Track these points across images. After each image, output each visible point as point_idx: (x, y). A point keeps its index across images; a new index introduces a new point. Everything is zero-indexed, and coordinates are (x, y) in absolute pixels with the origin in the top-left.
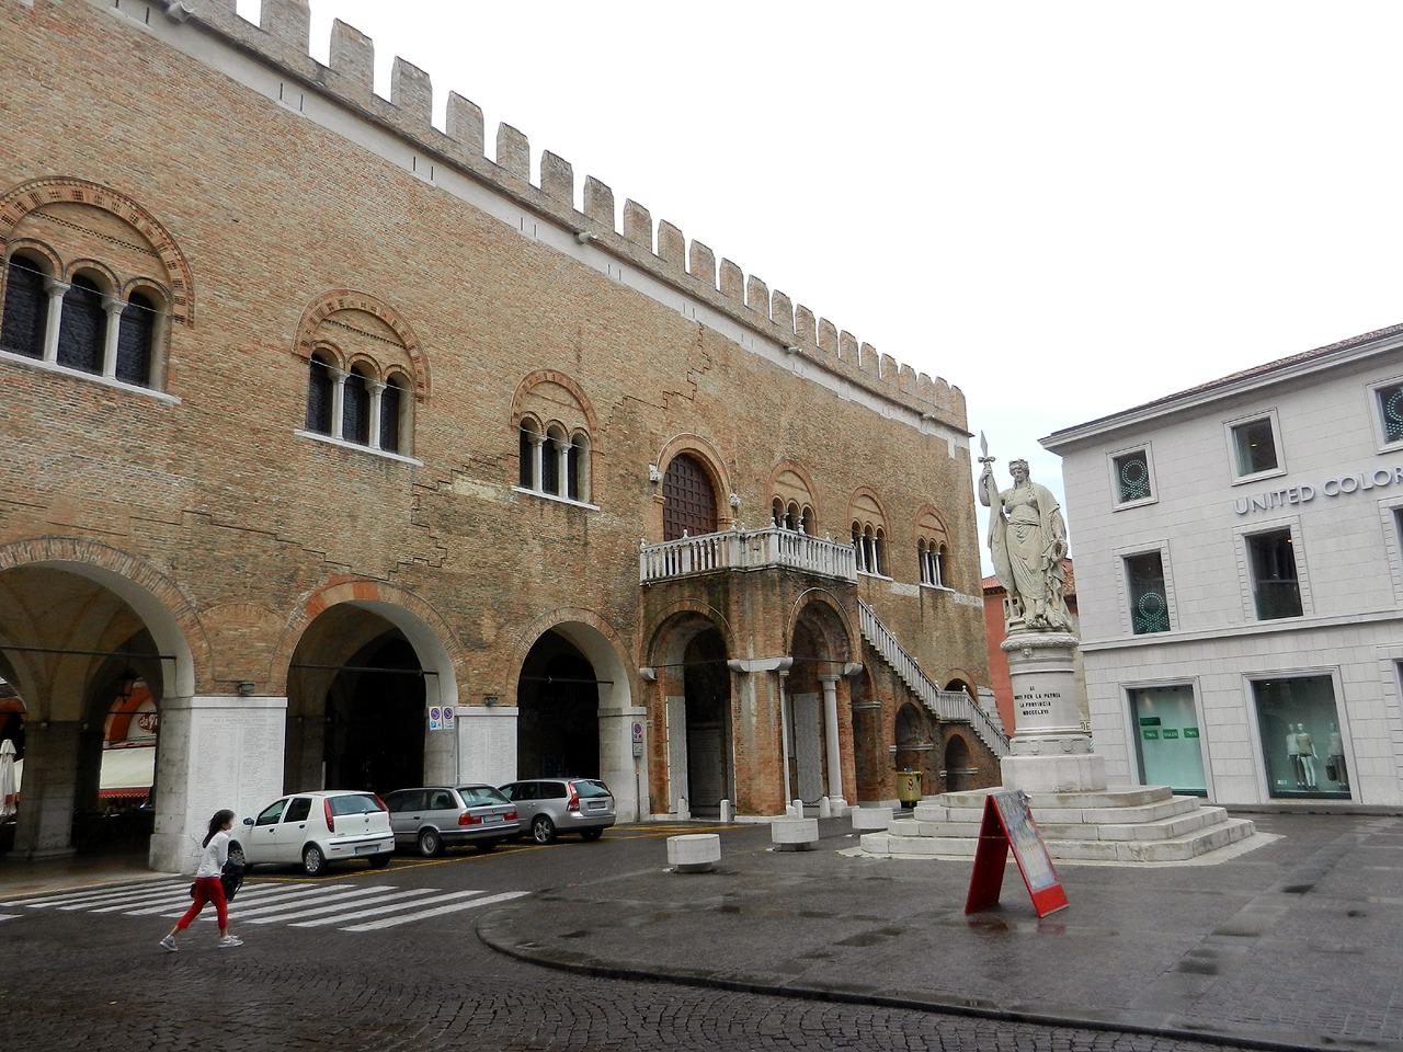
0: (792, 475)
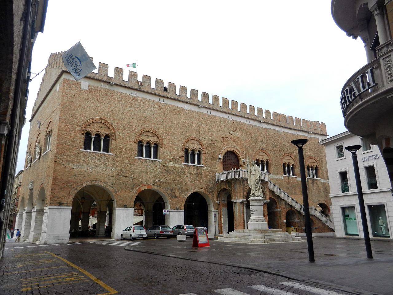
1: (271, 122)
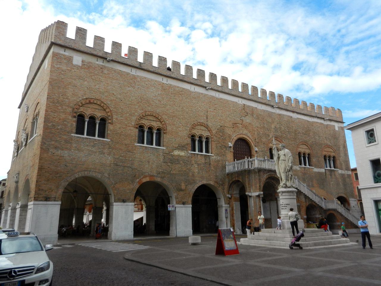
1: (285, 108)
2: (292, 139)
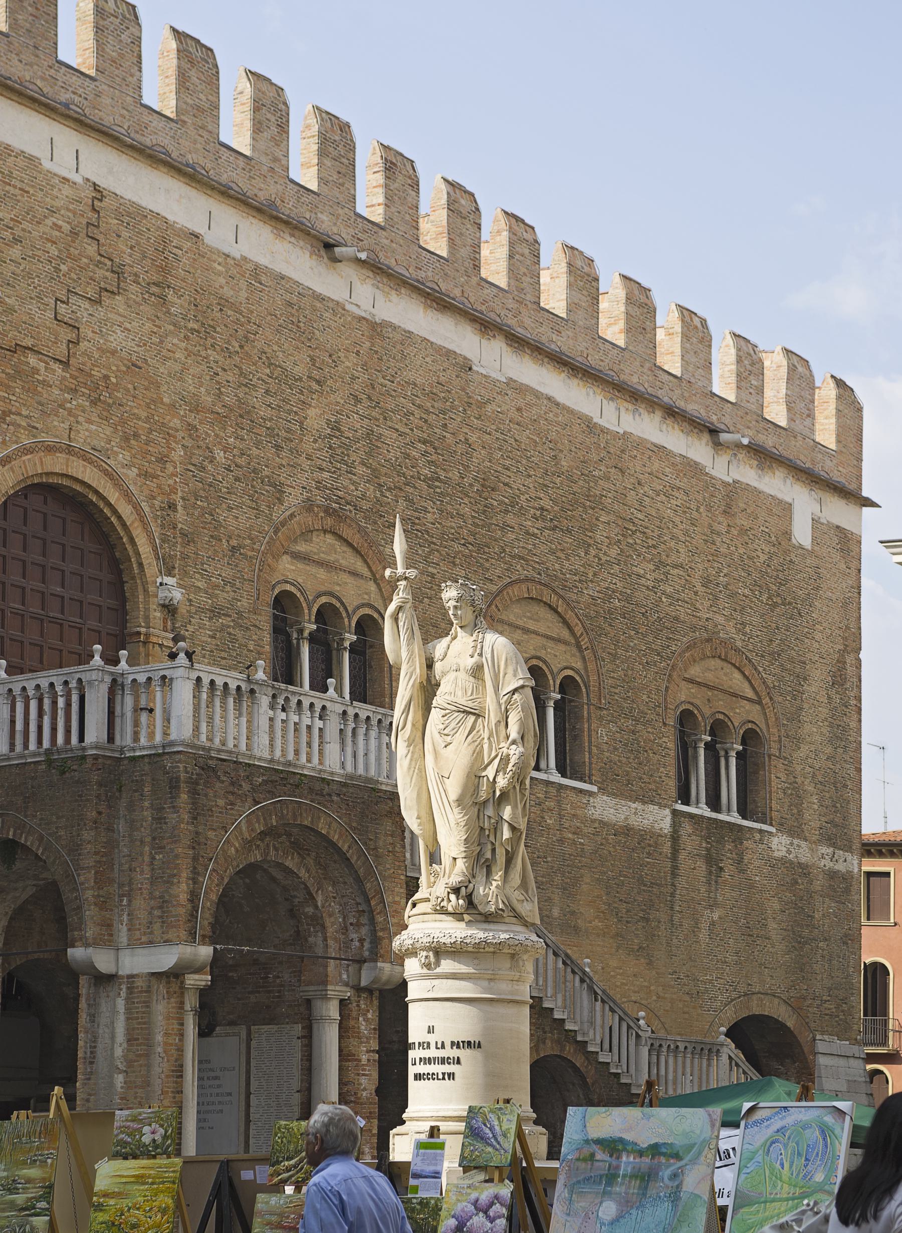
0: (330, 539)
1: (421, 275)
2: (457, 547)
